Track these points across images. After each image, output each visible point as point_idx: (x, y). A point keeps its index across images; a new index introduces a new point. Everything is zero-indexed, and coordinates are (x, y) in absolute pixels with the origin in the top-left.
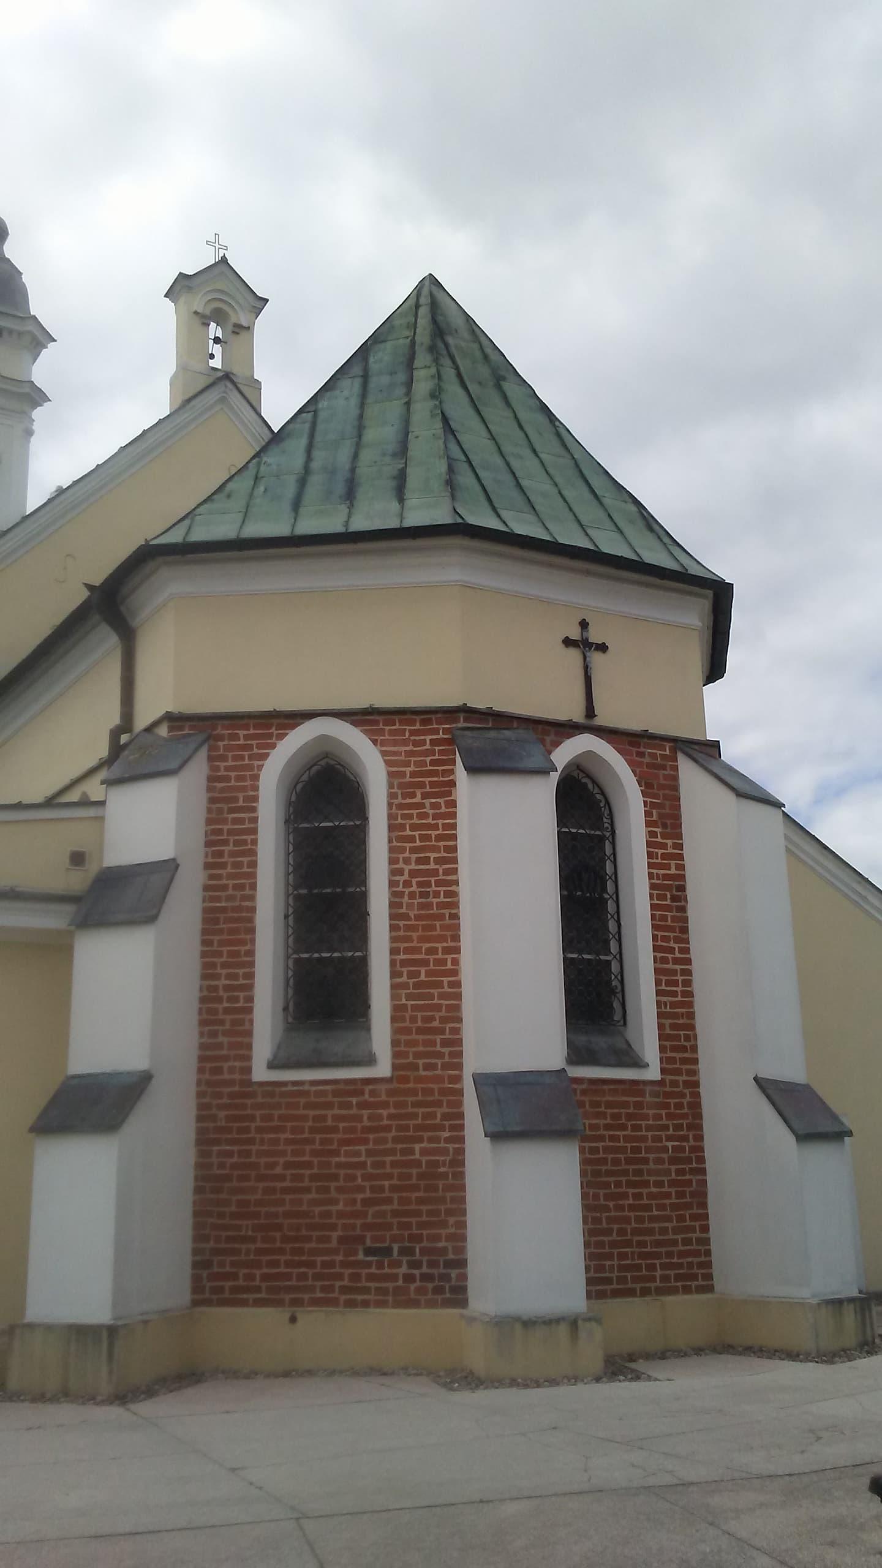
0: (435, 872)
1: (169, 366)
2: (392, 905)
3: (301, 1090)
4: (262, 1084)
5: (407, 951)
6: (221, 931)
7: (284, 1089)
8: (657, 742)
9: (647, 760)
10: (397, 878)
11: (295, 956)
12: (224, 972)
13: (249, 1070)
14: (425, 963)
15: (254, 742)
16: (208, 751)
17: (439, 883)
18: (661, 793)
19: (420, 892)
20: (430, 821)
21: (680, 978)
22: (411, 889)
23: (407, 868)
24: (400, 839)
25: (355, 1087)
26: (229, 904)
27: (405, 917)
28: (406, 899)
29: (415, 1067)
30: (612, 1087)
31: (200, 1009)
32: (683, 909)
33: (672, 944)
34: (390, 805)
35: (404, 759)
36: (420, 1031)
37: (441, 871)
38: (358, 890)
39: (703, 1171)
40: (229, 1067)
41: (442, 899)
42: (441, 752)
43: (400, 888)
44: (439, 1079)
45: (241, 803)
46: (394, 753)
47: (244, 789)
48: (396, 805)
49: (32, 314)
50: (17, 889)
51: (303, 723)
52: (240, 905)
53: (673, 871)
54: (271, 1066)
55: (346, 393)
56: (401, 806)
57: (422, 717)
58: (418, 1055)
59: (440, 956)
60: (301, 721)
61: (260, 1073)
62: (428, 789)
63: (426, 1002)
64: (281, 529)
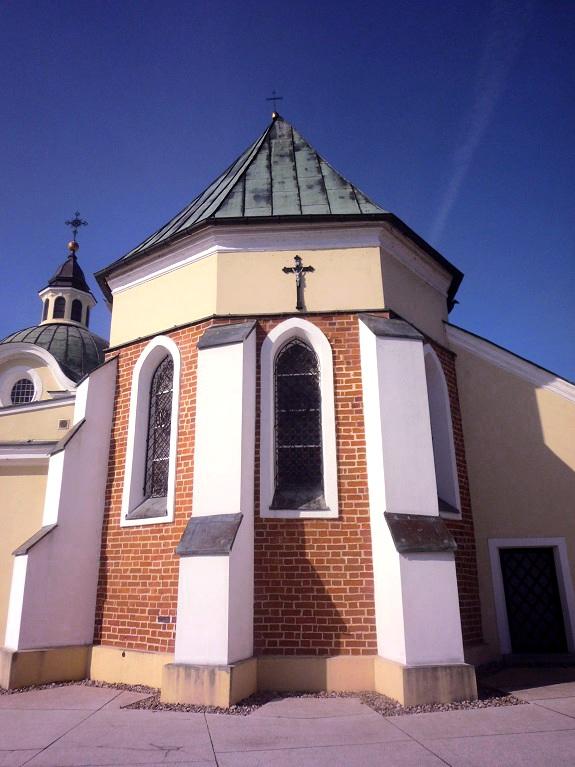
4: (267, 520)
9: (337, 326)
21: (357, 454)
27: (184, 433)
33: (352, 433)
39: (371, 575)
53: (354, 389)
54: (128, 518)
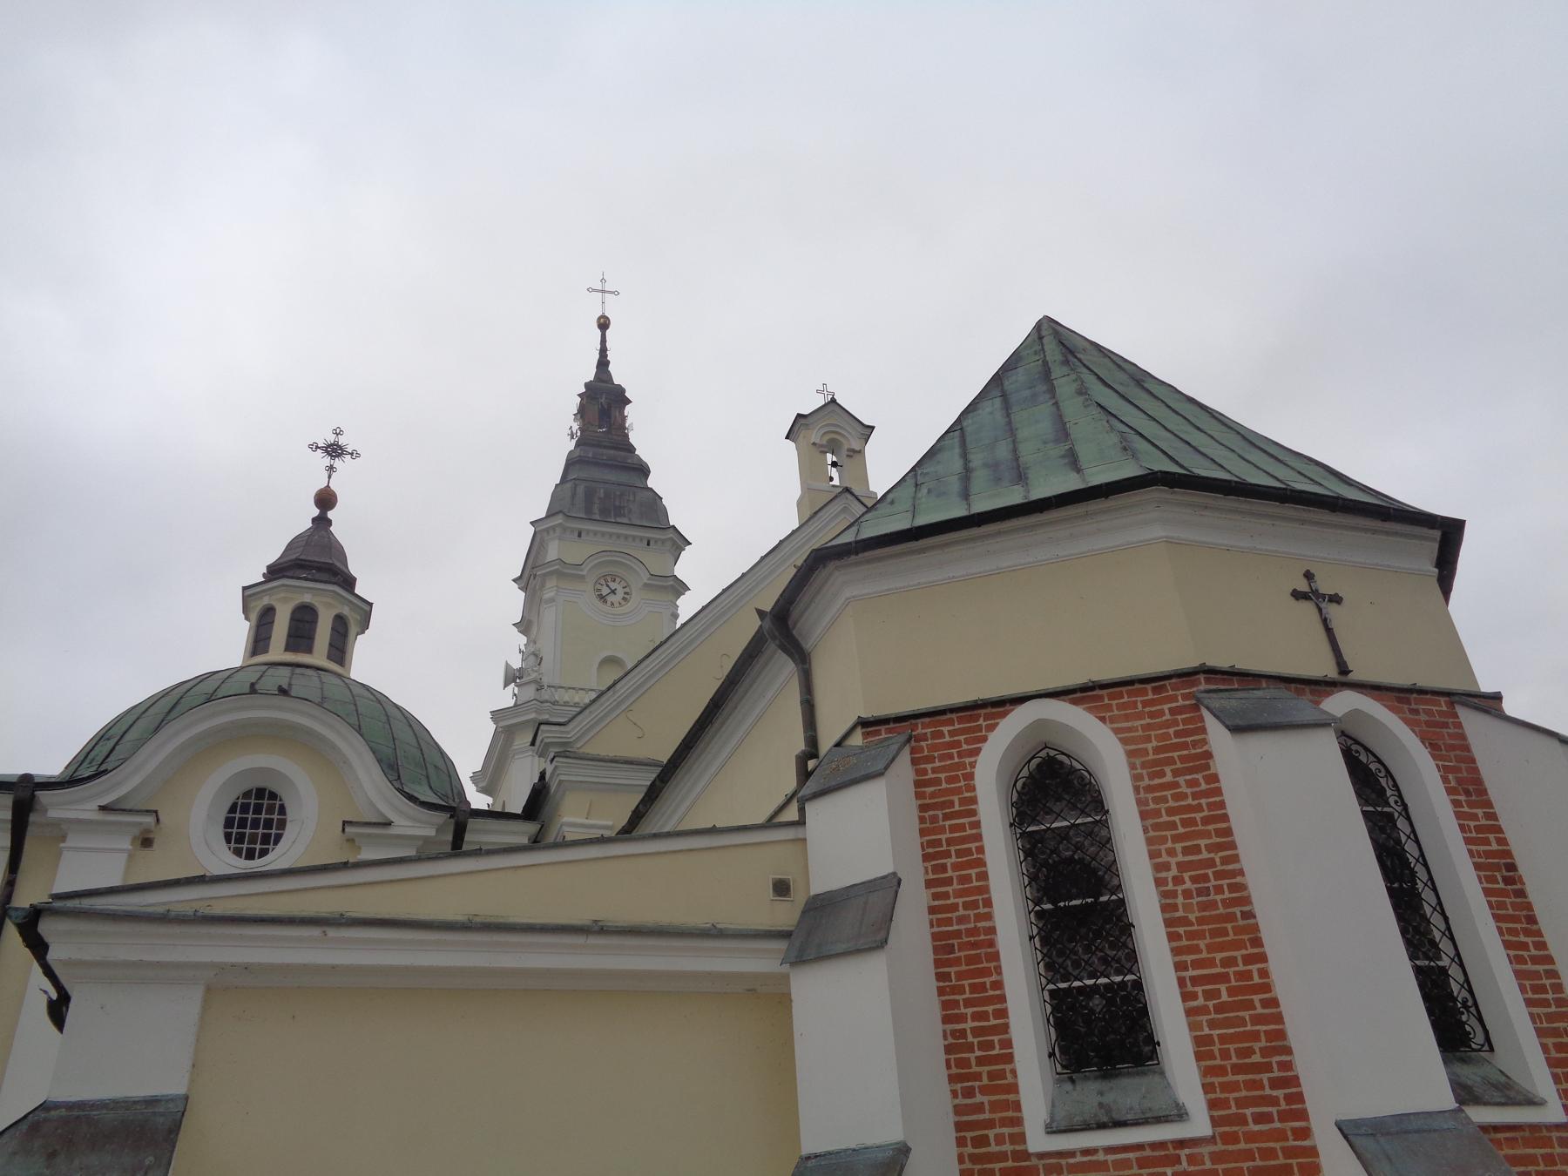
0: (1210, 863)
1: (795, 490)
2: (1165, 908)
3: (1095, 1161)
4: (1041, 1156)
5: (1197, 964)
6: (957, 961)
7: (1072, 1161)
8: (1428, 696)
9: (1423, 717)
10: (1163, 875)
11: (1051, 987)
12: (969, 1011)
13: (1020, 1138)
14: (1223, 978)
15: (962, 738)
16: (911, 754)
17: (1218, 875)
18: (1452, 754)
19: (1196, 889)
20: (1190, 801)
21: (1547, 982)
22: (1184, 887)
23: (1173, 861)
24: (1157, 827)
25: (1165, 1153)
26: (962, 927)
27: (1184, 921)
28: (1180, 900)
29: (1242, 1120)
30: (1508, 1135)
31: (948, 1062)
32: (1521, 893)
33: (1523, 938)
34: (1137, 789)
35: (1142, 734)
36: (1238, 1069)
37: (1218, 860)
38: (1114, 897)
40: (996, 1136)
41: (1227, 895)
42: (1185, 721)
43: (1170, 887)
44: (1280, 1135)
45: (957, 808)
46: (1129, 730)
47: (958, 791)
48: (1143, 787)
49: (671, 524)
50: (719, 926)
51: (1013, 710)
52: (976, 926)
54: (1052, 1130)
55: (988, 410)
56: (1149, 789)
57: (1153, 685)
58: (1241, 1103)
59: (1241, 967)
60: (1012, 707)
61: (1038, 1141)
62: (1179, 765)
63: (1237, 1030)
64: (958, 511)
